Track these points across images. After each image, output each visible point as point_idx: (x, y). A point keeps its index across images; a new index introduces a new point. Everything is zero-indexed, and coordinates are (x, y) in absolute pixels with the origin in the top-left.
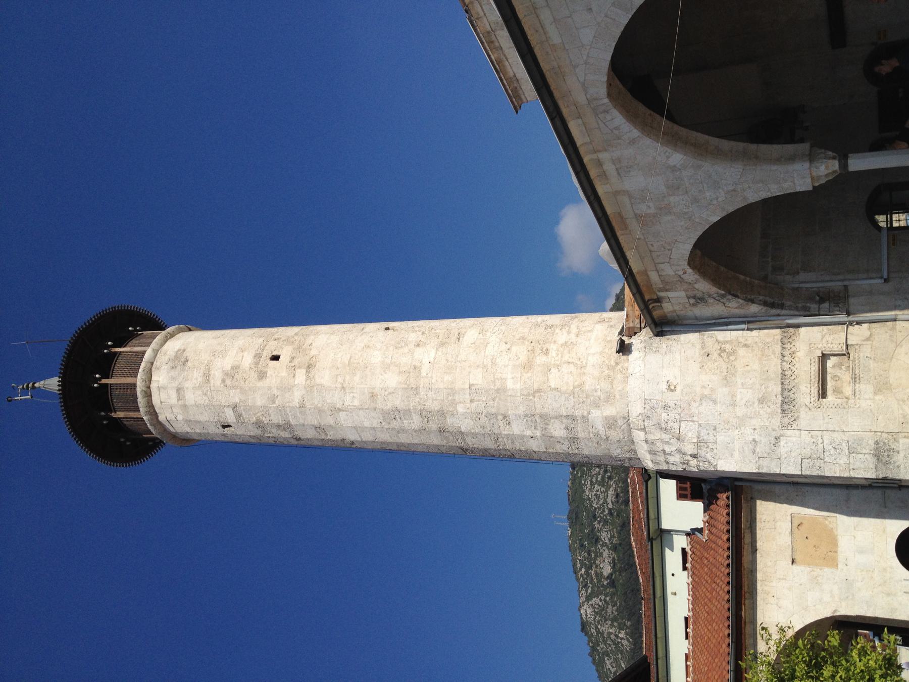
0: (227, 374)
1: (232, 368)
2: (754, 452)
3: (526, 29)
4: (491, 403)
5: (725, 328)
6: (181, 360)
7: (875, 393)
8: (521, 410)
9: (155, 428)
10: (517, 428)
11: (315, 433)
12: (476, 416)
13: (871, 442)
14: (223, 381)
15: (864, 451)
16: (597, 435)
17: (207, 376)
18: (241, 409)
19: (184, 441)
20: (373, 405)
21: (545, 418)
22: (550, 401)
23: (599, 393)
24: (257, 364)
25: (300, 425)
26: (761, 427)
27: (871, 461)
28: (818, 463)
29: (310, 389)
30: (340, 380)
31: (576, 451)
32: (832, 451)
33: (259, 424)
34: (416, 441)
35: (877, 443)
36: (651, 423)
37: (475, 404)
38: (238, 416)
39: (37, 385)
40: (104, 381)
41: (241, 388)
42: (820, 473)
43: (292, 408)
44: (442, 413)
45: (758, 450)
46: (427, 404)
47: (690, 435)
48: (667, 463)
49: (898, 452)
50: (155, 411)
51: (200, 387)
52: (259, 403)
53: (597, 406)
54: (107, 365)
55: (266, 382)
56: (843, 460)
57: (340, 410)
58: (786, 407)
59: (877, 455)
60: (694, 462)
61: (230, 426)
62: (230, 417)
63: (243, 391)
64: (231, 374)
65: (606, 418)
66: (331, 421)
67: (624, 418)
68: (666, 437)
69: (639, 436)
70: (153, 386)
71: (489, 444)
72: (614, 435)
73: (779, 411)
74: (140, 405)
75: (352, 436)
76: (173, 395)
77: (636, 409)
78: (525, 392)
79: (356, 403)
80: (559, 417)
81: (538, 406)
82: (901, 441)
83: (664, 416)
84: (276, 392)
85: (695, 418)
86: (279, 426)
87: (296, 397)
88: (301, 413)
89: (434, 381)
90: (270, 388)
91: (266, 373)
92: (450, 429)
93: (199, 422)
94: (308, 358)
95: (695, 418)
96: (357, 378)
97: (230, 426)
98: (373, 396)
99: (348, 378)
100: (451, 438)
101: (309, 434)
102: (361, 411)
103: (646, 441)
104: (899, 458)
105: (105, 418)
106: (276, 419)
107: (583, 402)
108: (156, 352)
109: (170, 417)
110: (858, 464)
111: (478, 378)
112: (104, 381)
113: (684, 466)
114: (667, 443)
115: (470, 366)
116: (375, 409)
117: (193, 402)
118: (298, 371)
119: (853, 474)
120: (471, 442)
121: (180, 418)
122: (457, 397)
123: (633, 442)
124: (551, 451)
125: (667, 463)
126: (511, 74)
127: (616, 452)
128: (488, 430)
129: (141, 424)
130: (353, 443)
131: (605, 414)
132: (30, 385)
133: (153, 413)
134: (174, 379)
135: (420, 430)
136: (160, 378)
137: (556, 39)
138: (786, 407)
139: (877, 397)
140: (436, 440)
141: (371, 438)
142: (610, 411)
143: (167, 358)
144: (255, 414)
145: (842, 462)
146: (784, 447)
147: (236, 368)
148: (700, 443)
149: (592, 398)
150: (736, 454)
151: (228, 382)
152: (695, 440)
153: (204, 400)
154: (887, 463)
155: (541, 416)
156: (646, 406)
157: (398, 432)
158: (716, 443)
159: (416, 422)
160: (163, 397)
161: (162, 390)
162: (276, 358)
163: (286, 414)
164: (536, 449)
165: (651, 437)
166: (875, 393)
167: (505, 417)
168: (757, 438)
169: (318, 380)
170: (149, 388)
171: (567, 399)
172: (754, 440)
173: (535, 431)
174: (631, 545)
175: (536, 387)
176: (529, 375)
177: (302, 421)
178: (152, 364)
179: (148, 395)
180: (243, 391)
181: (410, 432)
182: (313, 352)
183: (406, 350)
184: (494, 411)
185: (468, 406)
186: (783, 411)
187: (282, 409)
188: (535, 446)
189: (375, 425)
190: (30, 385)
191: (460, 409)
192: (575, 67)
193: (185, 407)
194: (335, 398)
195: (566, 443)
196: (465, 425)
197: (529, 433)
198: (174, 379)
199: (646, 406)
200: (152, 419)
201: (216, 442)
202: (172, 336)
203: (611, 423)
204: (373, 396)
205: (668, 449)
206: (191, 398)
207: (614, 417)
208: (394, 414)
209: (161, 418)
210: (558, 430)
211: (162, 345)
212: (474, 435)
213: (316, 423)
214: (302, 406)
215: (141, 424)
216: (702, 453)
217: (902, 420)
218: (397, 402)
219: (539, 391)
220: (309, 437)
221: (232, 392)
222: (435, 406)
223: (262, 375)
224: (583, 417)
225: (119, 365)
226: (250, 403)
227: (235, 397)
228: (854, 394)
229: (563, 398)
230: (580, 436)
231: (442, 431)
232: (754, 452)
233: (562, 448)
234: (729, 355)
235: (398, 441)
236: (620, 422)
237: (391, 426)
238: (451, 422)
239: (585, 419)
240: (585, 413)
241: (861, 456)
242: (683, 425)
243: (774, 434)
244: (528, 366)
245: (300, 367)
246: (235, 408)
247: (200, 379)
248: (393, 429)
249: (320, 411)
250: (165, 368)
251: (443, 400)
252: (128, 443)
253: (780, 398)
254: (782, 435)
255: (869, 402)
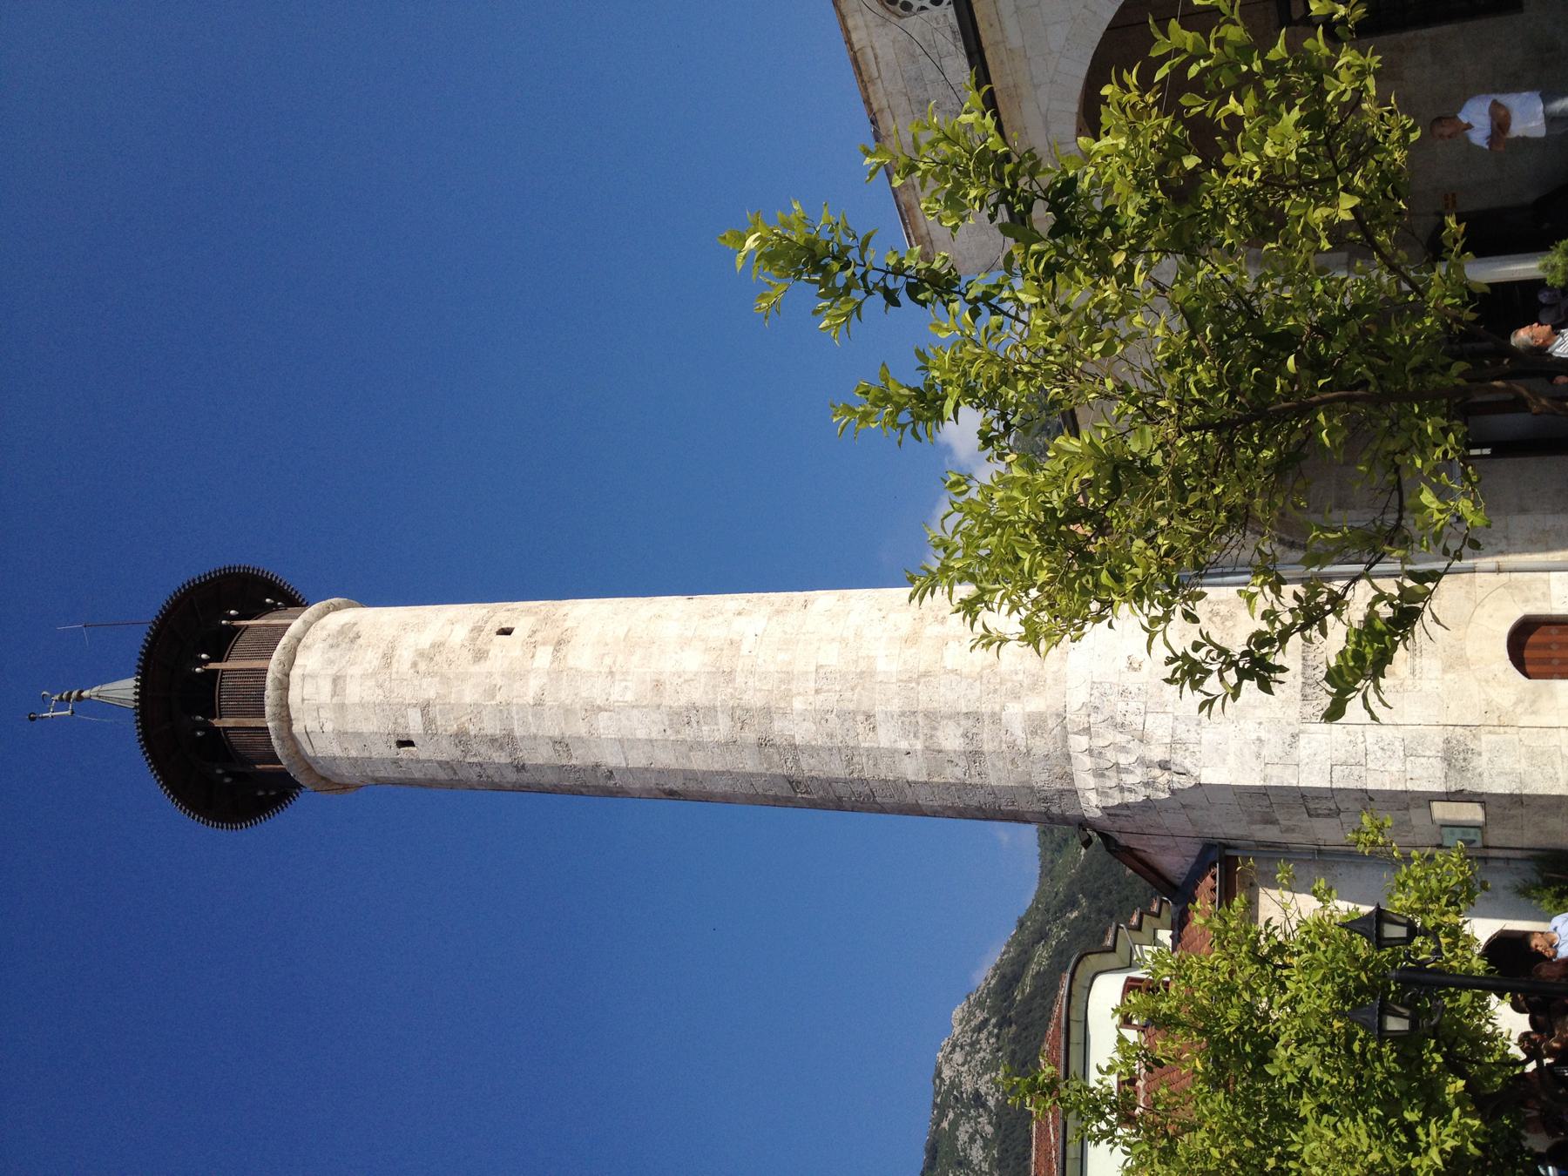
0: (421, 654)
1: (433, 646)
2: (1258, 756)
3: (978, 17)
4: (848, 694)
5: (1219, 580)
6: (350, 637)
7: (1444, 671)
8: (895, 706)
9: (283, 746)
10: (887, 737)
11: (552, 753)
12: (822, 717)
13: (1439, 740)
14: (415, 664)
15: (1428, 753)
16: (1012, 745)
17: (388, 659)
18: (434, 711)
19: (329, 782)
20: (656, 700)
21: (932, 717)
22: (942, 690)
23: (1020, 677)
24: (474, 640)
25: (529, 737)
26: (1271, 720)
27: (1438, 768)
28: (1356, 770)
29: (555, 675)
30: (608, 661)
31: (976, 780)
32: (1379, 753)
33: (461, 738)
34: (717, 767)
35: (1447, 741)
36: (1101, 718)
37: (821, 697)
38: (428, 722)
39: (86, 694)
40: (212, 666)
41: (442, 676)
42: (1360, 785)
43: (522, 707)
44: (767, 712)
45: (1264, 752)
46: (746, 697)
47: (1159, 732)
48: (1122, 790)
49: (1480, 754)
50: (289, 715)
51: (374, 674)
52: (468, 700)
53: (1018, 698)
54: (221, 644)
55: (484, 667)
56: (1395, 767)
57: (600, 709)
58: (1309, 691)
59: (1448, 758)
60: (1163, 778)
61: (410, 743)
62: (414, 725)
63: (445, 680)
64: (428, 655)
65: (1030, 717)
66: (581, 729)
67: (1058, 715)
68: (1121, 739)
69: (1079, 743)
70: (295, 673)
71: (837, 770)
72: (1041, 745)
73: (1299, 697)
74: (267, 709)
75: (612, 759)
76: (326, 687)
77: (1077, 698)
78: (905, 677)
79: (629, 697)
80: (954, 716)
81: (923, 697)
82: (1484, 738)
83: (1121, 706)
84: (499, 681)
85: (1169, 709)
86: (493, 740)
87: (533, 686)
88: (535, 715)
89: (760, 661)
90: (490, 674)
91: (487, 652)
92: (778, 741)
93: (361, 734)
94: (559, 631)
95: (1169, 709)
96: (635, 659)
97: (410, 743)
98: (658, 685)
99: (620, 658)
100: (776, 757)
101: (541, 756)
102: (635, 711)
103: (1090, 751)
104: (1481, 763)
105: (198, 726)
106: (491, 727)
107: (995, 691)
108: (308, 626)
109: (312, 725)
110: (1418, 772)
111: (831, 657)
112: (212, 666)
113: (1149, 792)
114: (1123, 749)
115: (821, 640)
116: (659, 707)
117: (357, 700)
118: (540, 649)
119: (1411, 786)
120: (809, 766)
121: (328, 727)
122: (794, 687)
123: (1068, 757)
124: (936, 780)
125: (1122, 790)
126: (923, 231)
127: (1040, 779)
128: (837, 742)
129: (259, 739)
130: (610, 774)
131: (1028, 710)
132: (75, 694)
133: (286, 718)
134: (332, 662)
135: (727, 744)
136: (307, 661)
137: (1015, 40)
138: (1309, 691)
139: (1449, 676)
140: (750, 764)
141: (643, 763)
142: (1036, 704)
143: (325, 633)
144: (456, 719)
145: (1394, 769)
146: (1304, 749)
147: (438, 646)
148: (1174, 743)
149: (1009, 685)
150: (1231, 760)
151: (422, 666)
152: (1168, 740)
153: (377, 696)
154: (1463, 770)
155: (927, 715)
156: (1095, 692)
157: (691, 748)
158: (1199, 743)
159: (722, 729)
160: (309, 690)
161: (308, 680)
162: (506, 632)
163: (510, 717)
164: (911, 778)
165: (1099, 743)
166: (1444, 671)
167: (868, 717)
168: (1264, 736)
169: (571, 662)
170: (288, 675)
171: (971, 686)
172: (1259, 739)
173: (914, 741)
174: (1029, 1132)
175: (922, 669)
176: (913, 650)
177: (533, 730)
178: (299, 640)
179: (283, 685)
180: (445, 680)
181: (712, 752)
182: (568, 624)
183: (720, 619)
184: (852, 707)
185: (811, 699)
186: (1305, 697)
187: (503, 710)
188: (911, 770)
189: (654, 736)
190: (75, 694)
191: (798, 704)
192: (1036, 87)
193: (342, 708)
194: (595, 691)
195: (963, 763)
196: (802, 732)
197: (903, 745)
198: (332, 662)
199: (1095, 692)
200: (281, 729)
201: (378, 782)
202: (337, 608)
203: (1036, 725)
204: (658, 685)
205: (1123, 760)
206: (355, 692)
207: (1041, 714)
208: (689, 714)
209: (297, 728)
210: (951, 739)
211: (319, 617)
212: (814, 751)
213: (556, 733)
214: (539, 704)
215: (259, 739)
216: (1178, 758)
217: (1484, 708)
218: (697, 694)
219: (926, 674)
220: (541, 762)
221: (426, 682)
222: (754, 699)
223: (480, 656)
224: (993, 714)
225: (241, 644)
226: (453, 699)
227: (429, 690)
228: (1413, 673)
229: (964, 684)
230: (985, 748)
231: (763, 744)
232: (1258, 756)
233: (953, 774)
234: (1224, 619)
235: (688, 766)
236: (1051, 723)
237: (680, 737)
238: (781, 728)
239: (996, 718)
240: (997, 708)
241: (1423, 760)
242: (1150, 718)
243: (1291, 730)
244: (911, 639)
245: (544, 644)
246: (425, 708)
247: (376, 663)
248: (684, 741)
249: (568, 711)
250: (320, 645)
251: (770, 691)
252: (227, 780)
253: (1300, 679)
254: (1301, 732)
255: (1435, 683)
